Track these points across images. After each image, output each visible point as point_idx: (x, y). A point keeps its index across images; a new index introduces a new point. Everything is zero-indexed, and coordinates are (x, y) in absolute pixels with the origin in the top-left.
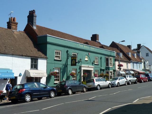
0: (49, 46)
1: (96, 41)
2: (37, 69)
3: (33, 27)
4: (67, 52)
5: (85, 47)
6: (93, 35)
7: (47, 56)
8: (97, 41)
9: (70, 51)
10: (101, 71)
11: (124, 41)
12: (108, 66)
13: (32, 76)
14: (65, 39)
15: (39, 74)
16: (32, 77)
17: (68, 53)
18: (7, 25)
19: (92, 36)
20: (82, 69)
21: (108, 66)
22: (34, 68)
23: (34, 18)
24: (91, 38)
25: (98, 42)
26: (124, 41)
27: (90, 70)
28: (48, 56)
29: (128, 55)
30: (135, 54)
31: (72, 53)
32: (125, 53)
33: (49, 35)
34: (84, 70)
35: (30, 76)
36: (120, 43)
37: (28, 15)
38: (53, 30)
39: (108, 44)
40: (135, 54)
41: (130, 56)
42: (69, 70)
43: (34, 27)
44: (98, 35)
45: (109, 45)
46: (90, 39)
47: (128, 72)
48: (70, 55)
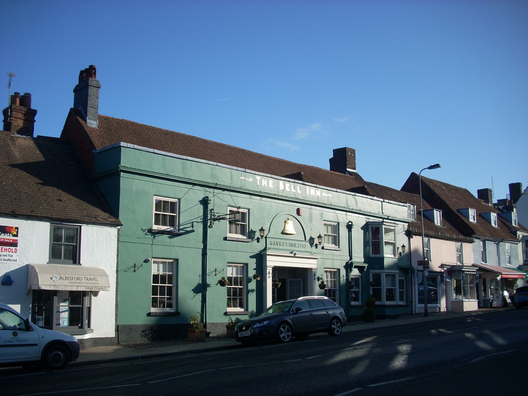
0: (125, 180)
1: (345, 171)
2: (75, 263)
3: (86, 121)
4: (205, 202)
5: (284, 185)
6: (335, 152)
7: (118, 217)
8: (348, 169)
9: (217, 200)
10: (76, 245)
11: (437, 166)
12: (379, 253)
13: (43, 287)
14: (169, 152)
15: (78, 279)
16: (44, 290)
17: (210, 207)
18: (3, 119)
19: (332, 156)
20: (268, 264)
21: (379, 253)
22: (65, 258)
23: (520, 187)
24: (331, 160)
25: (350, 173)
26: (437, 166)
27: (306, 269)
28: (121, 218)
29: (463, 218)
30: (492, 213)
31: (155, 198)
32: (454, 209)
33: (129, 145)
34: (276, 269)
35: (36, 288)
36: (422, 174)
37: (78, 83)
38: (166, 133)
39: (398, 184)
40: (492, 213)
41: (471, 220)
42: (268, 272)
43: (88, 121)
44: (355, 150)
45: (399, 188)
46: (326, 166)
47: (3, 240)
48: (217, 215)
